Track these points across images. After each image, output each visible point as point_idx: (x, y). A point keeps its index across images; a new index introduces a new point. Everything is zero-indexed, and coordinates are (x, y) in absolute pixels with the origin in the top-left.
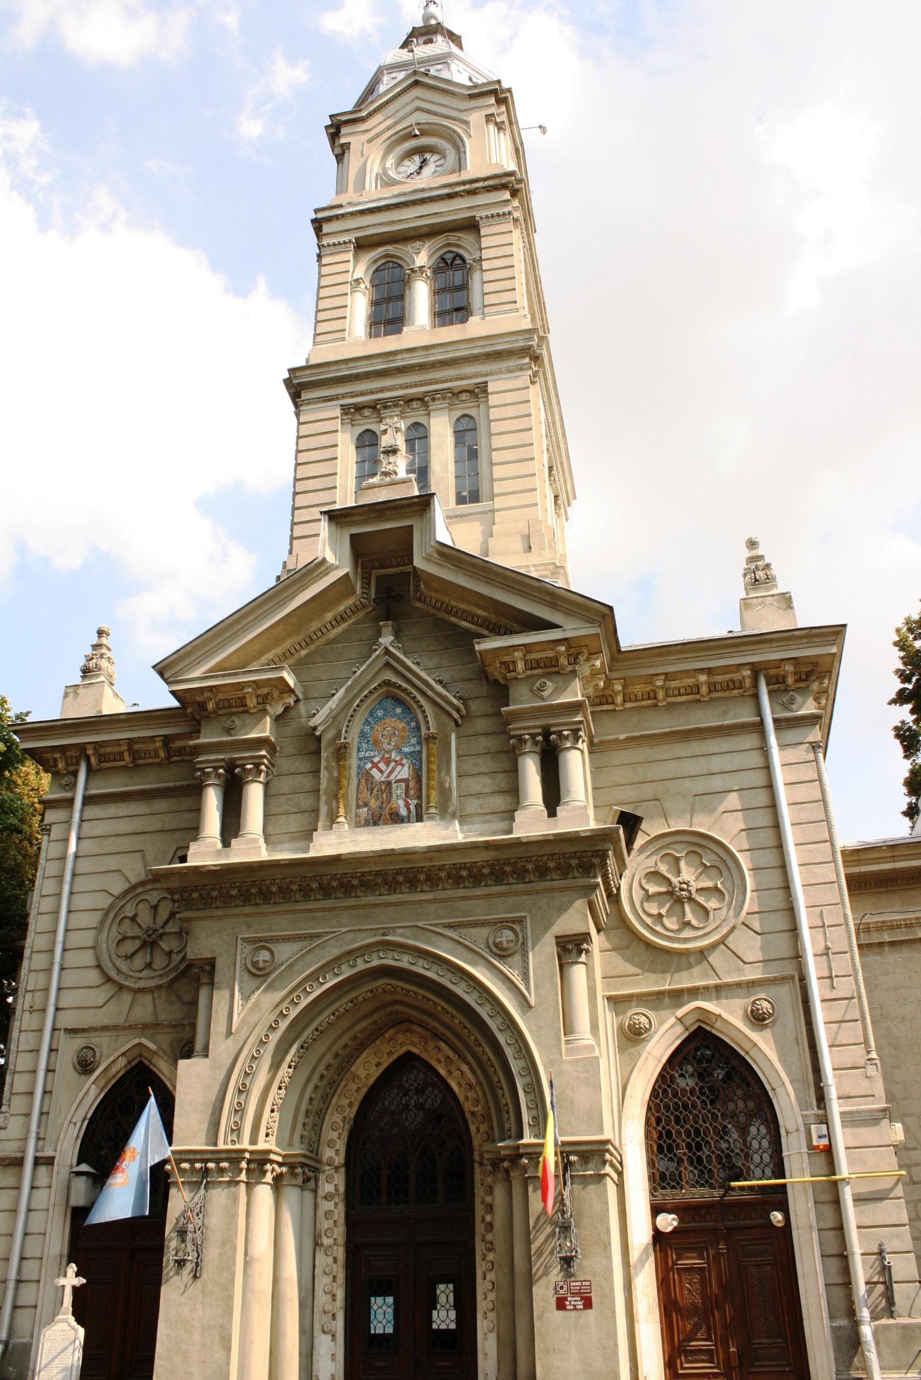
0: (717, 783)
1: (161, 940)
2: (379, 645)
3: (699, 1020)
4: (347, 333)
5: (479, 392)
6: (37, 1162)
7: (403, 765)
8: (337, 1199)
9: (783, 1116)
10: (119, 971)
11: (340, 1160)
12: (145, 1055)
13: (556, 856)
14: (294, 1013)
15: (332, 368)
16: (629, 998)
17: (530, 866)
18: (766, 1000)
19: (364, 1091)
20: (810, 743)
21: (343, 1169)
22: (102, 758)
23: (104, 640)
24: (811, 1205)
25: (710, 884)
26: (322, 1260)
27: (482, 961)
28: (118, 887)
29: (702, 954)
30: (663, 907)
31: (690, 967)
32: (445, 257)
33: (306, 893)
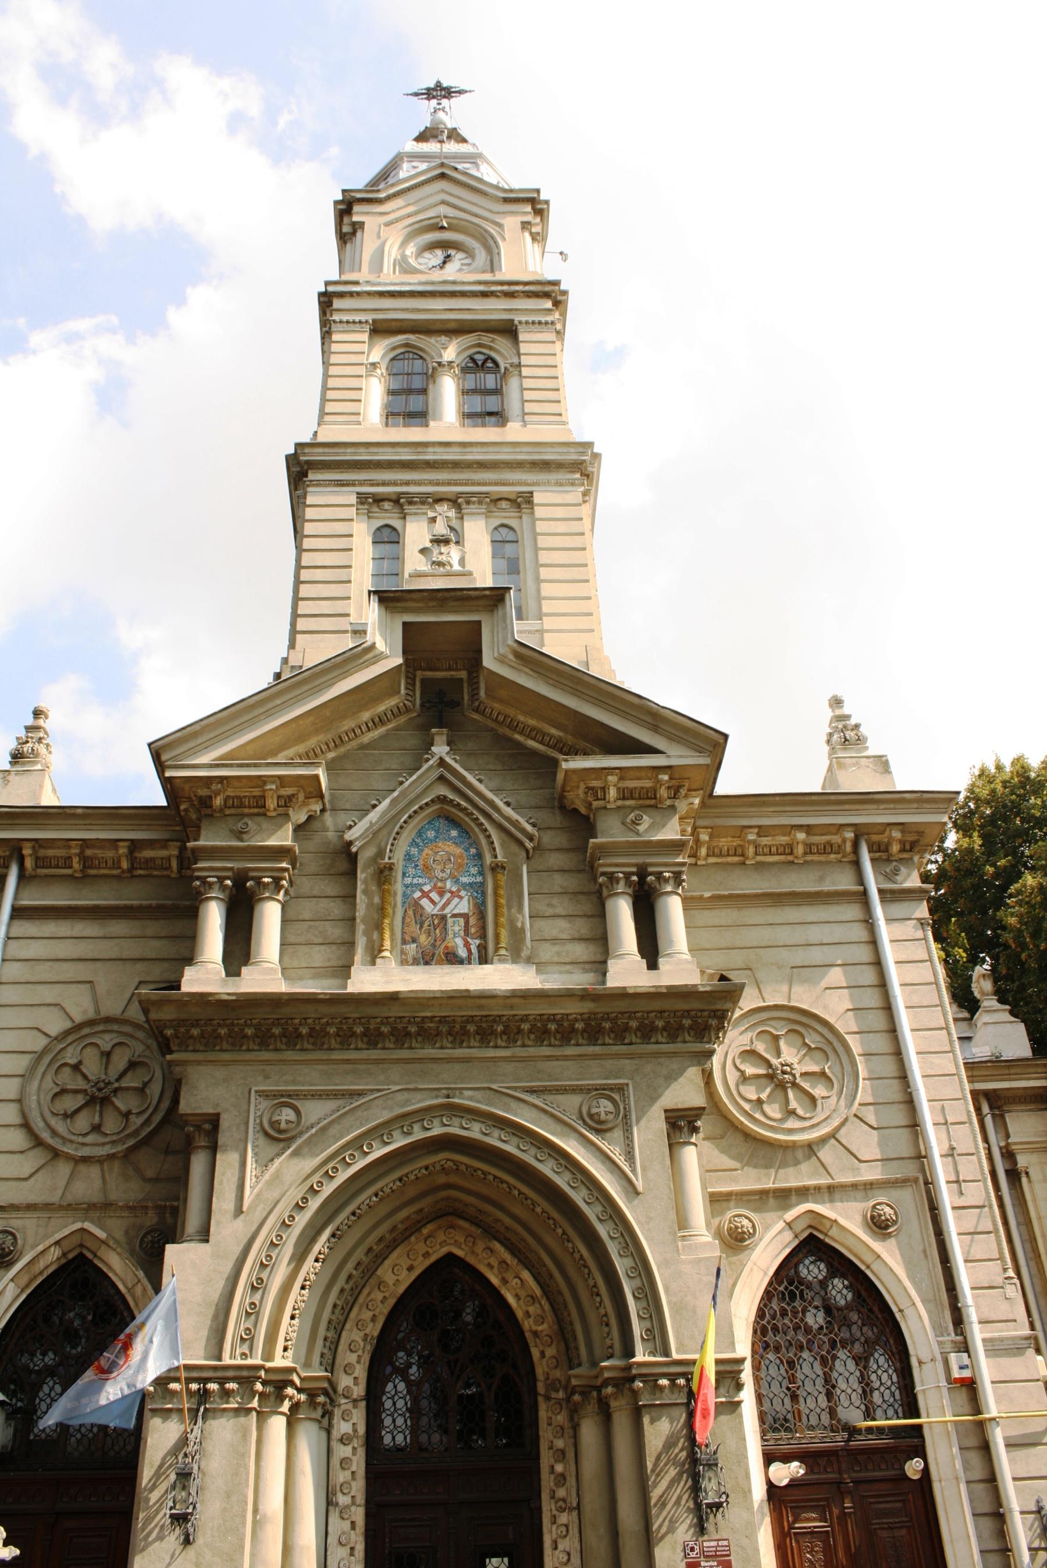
0: (817, 955)
1: (115, 1096)
2: (433, 755)
3: (810, 1226)
4: (361, 417)
5: (523, 502)
7: (461, 898)
8: (355, 1443)
9: (914, 1342)
10: (54, 1133)
12: (88, 1245)
13: (666, 1014)
15: (349, 450)
17: (634, 1024)
18: (888, 1205)
19: (391, 1302)
20: (918, 919)
21: (363, 1404)
22: (41, 862)
23: (41, 722)
24: (955, 1450)
25: (816, 1068)
26: (337, 1526)
27: (574, 1135)
28: (56, 1025)
29: (811, 1148)
30: (763, 1091)
31: (797, 1163)
32: (476, 357)
33: (346, 1038)
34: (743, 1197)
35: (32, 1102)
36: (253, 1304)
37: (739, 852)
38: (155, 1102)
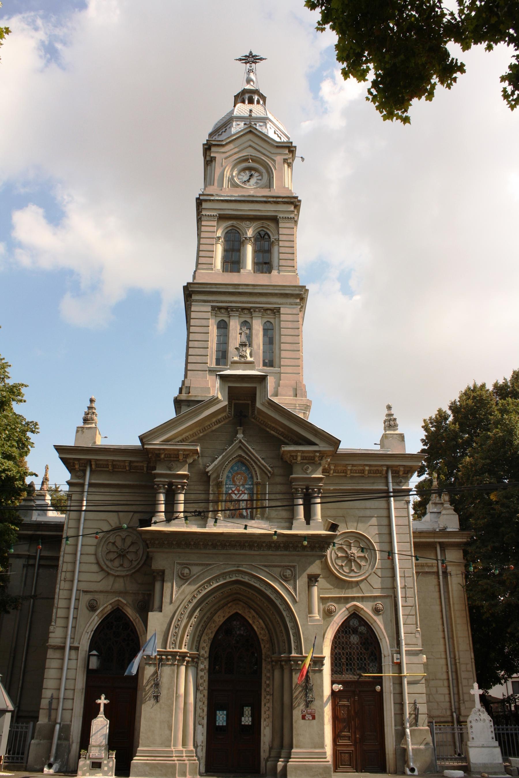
0: (368, 513)
3: (354, 610)
5: (276, 312)
6: (71, 648)
10: (108, 567)
11: (206, 655)
14: (199, 596)
15: (208, 286)
16: (328, 598)
22: (96, 465)
24: (391, 684)
29: (357, 583)
31: (352, 588)
33: (205, 546)
34: (333, 599)
35: (100, 555)
36: (175, 632)
37: (345, 471)
38: (140, 557)
